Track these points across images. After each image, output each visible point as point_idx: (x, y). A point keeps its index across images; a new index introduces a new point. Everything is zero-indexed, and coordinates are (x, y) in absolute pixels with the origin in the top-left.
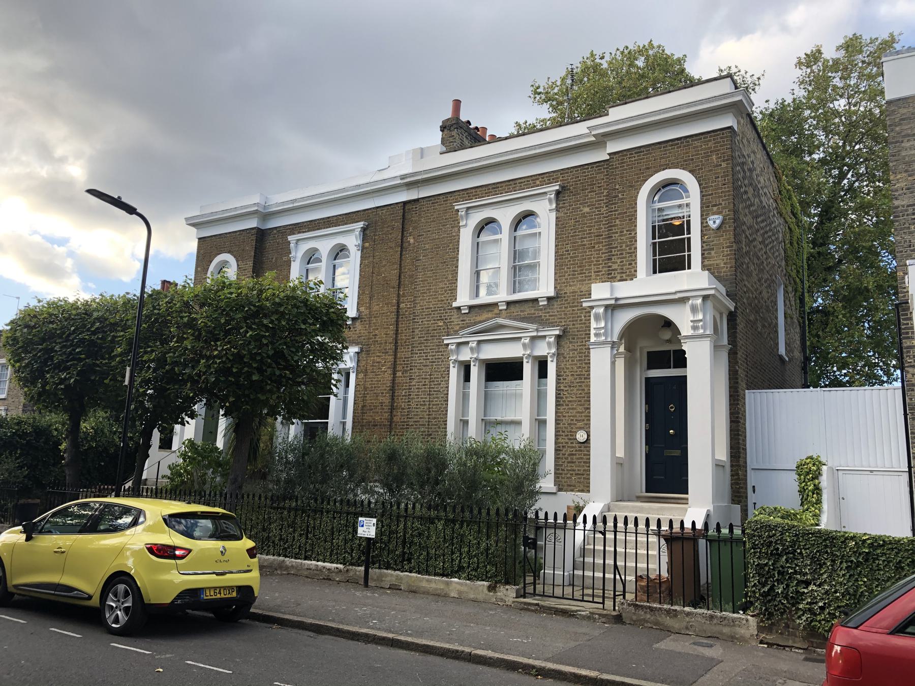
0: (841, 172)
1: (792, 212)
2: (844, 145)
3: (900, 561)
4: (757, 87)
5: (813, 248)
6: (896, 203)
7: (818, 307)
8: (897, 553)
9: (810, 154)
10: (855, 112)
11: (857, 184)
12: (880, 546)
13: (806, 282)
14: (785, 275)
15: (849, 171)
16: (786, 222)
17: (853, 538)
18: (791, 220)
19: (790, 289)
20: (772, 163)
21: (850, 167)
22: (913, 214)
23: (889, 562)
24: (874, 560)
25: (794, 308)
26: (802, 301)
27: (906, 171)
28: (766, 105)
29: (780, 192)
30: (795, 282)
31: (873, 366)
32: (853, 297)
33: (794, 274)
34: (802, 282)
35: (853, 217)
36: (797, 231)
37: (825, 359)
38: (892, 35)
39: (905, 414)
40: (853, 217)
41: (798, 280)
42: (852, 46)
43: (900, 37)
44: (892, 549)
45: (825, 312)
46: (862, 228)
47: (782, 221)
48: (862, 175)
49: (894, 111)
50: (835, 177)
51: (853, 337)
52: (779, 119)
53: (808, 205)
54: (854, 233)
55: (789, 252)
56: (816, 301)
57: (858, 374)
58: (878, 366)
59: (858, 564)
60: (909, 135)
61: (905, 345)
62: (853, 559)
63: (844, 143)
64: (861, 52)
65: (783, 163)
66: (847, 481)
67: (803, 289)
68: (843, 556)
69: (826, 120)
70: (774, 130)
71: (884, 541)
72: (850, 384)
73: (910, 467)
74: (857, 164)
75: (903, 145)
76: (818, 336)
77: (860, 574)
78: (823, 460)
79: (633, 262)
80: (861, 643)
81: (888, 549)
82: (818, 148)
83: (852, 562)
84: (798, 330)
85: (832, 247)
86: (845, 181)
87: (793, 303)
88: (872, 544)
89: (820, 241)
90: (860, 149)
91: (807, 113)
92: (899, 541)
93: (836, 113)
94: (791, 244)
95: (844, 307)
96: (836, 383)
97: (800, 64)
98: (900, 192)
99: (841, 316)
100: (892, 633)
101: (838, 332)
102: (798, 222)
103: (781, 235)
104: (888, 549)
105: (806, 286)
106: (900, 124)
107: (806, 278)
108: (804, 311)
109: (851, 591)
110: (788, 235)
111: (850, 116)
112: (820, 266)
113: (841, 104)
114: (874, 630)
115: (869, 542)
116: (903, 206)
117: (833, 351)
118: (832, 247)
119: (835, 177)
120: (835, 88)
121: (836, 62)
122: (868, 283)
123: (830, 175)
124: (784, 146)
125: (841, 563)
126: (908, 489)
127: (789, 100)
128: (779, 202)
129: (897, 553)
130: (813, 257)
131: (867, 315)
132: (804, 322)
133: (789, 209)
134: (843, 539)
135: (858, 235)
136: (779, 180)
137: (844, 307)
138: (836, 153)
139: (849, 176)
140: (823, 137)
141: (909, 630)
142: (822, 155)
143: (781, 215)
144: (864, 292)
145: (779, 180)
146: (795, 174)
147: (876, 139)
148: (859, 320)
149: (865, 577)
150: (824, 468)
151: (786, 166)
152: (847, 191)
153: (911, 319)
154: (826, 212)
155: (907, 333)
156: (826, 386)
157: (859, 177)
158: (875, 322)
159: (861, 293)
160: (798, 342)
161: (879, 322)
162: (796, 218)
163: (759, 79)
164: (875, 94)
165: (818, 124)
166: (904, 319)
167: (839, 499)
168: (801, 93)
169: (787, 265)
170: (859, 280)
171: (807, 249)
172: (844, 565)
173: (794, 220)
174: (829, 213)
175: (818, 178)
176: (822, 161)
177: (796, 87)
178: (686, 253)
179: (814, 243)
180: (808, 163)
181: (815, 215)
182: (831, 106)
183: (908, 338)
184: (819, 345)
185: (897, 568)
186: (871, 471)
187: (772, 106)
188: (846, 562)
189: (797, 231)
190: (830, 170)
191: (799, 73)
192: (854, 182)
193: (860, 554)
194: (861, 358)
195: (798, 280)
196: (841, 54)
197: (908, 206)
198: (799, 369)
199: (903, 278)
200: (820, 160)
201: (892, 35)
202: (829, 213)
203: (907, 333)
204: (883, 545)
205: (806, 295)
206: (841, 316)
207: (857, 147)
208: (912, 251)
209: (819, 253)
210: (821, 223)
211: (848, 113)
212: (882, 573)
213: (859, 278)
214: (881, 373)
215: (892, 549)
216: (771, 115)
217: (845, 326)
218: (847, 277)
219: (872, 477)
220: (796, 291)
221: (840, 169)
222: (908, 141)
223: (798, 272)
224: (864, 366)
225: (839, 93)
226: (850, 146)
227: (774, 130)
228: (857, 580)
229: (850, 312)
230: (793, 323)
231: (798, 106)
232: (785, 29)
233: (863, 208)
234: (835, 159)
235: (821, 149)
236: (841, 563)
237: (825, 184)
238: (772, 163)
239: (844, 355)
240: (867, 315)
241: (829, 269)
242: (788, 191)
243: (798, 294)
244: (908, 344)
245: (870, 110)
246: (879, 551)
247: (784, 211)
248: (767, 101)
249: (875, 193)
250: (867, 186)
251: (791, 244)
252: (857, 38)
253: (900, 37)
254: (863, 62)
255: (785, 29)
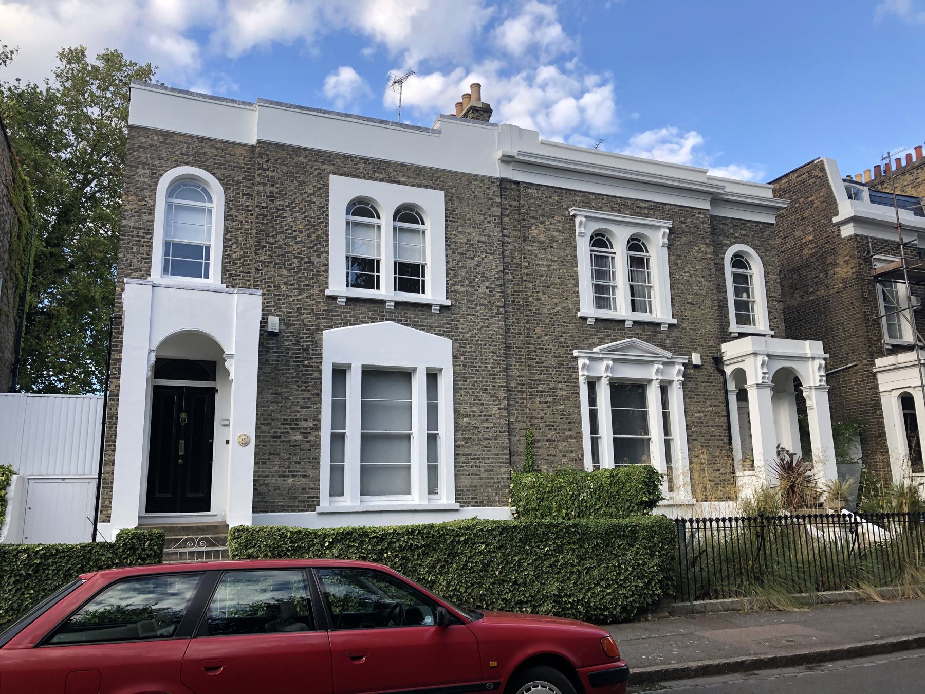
0: (85, 178)
1: (25, 205)
2: (91, 154)
3: (70, 568)
4: (8, 61)
5: (46, 247)
6: (125, 222)
7: (43, 308)
8: (68, 561)
9: (57, 150)
10: (107, 126)
11: (98, 195)
12: (52, 555)
13: (30, 280)
14: (7, 269)
15: (93, 180)
16: (17, 214)
17: (25, 551)
18: (23, 213)
19: (10, 285)
20: (9, 147)
21: (95, 176)
22: (2, 215)
23: (58, 571)
24: (44, 570)
25: (11, 306)
26: (22, 299)
27: (137, 195)
28: (17, 84)
29: (14, 180)
30: (17, 279)
31: (88, 374)
32: (79, 304)
33: (17, 270)
34: (26, 280)
35: (91, 225)
36: (27, 226)
37: (42, 363)
38: (149, 66)
39: (104, 423)
40: (91, 225)
41: (20, 277)
42: (112, 59)
43: (156, 71)
44: (64, 557)
45: (49, 314)
46: (97, 238)
47: (11, 211)
48: (105, 187)
49: (134, 137)
50: (78, 181)
51: (73, 343)
52: (28, 103)
53: (47, 202)
54: (89, 241)
55: (15, 246)
56: (41, 302)
57: (74, 381)
58: (94, 374)
59: (28, 576)
60: (144, 164)
61: (112, 357)
62: (22, 572)
63: (92, 152)
64: (119, 70)
65: (26, 151)
66: (40, 491)
67: (25, 287)
68: (13, 570)
69: (79, 121)
70: (21, 114)
71: (57, 550)
72: (64, 391)
73: (100, 474)
74: (101, 175)
75: (138, 170)
76: (38, 338)
77: (26, 587)
78: (14, 469)
79: (148, 260)
80: (8, 662)
81: (60, 558)
82: (66, 148)
83: (21, 575)
84: (13, 329)
85: (66, 250)
86: (88, 189)
87: (11, 300)
88: (45, 554)
89: (55, 241)
90: (106, 163)
91: (60, 108)
92: (72, 548)
93: (88, 119)
94: (19, 237)
95: (69, 313)
96: (50, 389)
97: (62, 55)
98: (129, 213)
99: (65, 321)
100: (35, 647)
101: (59, 336)
102: (31, 217)
103: (8, 226)
104: (60, 558)
105: (29, 285)
106: (138, 151)
107: (31, 276)
108: (23, 311)
109: (16, 605)
110: (16, 228)
111: (101, 127)
112: (49, 266)
113: (94, 112)
114: (20, 647)
115: (41, 552)
116: (130, 227)
117: (53, 355)
118: (66, 250)
119: (78, 181)
120: (92, 94)
121: (96, 70)
122: (95, 292)
123: (74, 179)
124: (30, 134)
125: (9, 578)
126: (95, 495)
127: (42, 88)
128: (11, 189)
129: (68, 561)
130: (45, 256)
131: (91, 323)
132: (21, 322)
133: (21, 200)
134: (15, 553)
135: (92, 245)
136: (15, 167)
137: (69, 313)
138: (83, 158)
139: (93, 184)
140: (73, 139)
141: (55, 640)
142: (69, 156)
143: (11, 204)
144: (90, 302)
145: (15, 167)
146: (37, 166)
147: (122, 157)
148: (83, 328)
149: (32, 589)
150: (14, 478)
151: (29, 155)
152: (88, 199)
153: (122, 333)
154: (66, 214)
155: (117, 346)
156: (39, 391)
157: (101, 188)
158: (96, 331)
159: (87, 302)
160: (11, 343)
161: (99, 332)
162: (28, 211)
163: (12, 52)
164: (124, 117)
165: (69, 123)
166: (116, 333)
167: (25, 508)
168: (56, 85)
169: (10, 259)
170: (88, 288)
171: (37, 246)
172: (13, 579)
173: (26, 213)
174: (67, 215)
175: (60, 176)
176: (68, 163)
177: (52, 77)
178: (171, 258)
179: (48, 242)
180: (53, 159)
181: (53, 214)
182: (85, 110)
183: (117, 351)
184: (38, 347)
185: (65, 575)
186: (63, 479)
187: (23, 87)
188: (15, 576)
189: (27, 226)
190: (75, 173)
191: (62, 65)
192: (97, 192)
193: (31, 566)
194: (79, 365)
195: (20, 277)
196: (100, 64)
197: (134, 228)
198: (8, 371)
199: (121, 294)
200: (65, 160)
201: (149, 66)
202: (67, 215)
203: (117, 346)
204: (56, 554)
205: (28, 293)
206: (65, 321)
207: (104, 159)
208: (132, 270)
209: (51, 253)
210: (58, 223)
211: (100, 124)
212: (50, 582)
213: (88, 286)
214: (95, 381)
215: (64, 557)
216: (20, 95)
217: (68, 332)
218: (76, 284)
219: (63, 485)
220: (17, 288)
221: (85, 175)
222: (143, 168)
223: (22, 268)
224: (80, 373)
225: (95, 101)
226: (98, 155)
227: (21, 114)
228: (23, 594)
229: (75, 318)
230: (8, 321)
231: (51, 99)
232: (55, 14)
233: (101, 219)
234: (81, 164)
235: (69, 150)
236: (9, 578)
237: (67, 186)
238: (9, 147)
239: (62, 360)
240: (91, 323)
241: (59, 272)
242: (23, 181)
243: (18, 292)
244: (116, 357)
245: (120, 128)
246: (50, 561)
247: (15, 201)
248: (18, 80)
249: (114, 209)
250: (108, 199)
251: (19, 237)
252: (118, 55)
253: (156, 71)
254: (120, 81)
255: (55, 14)
